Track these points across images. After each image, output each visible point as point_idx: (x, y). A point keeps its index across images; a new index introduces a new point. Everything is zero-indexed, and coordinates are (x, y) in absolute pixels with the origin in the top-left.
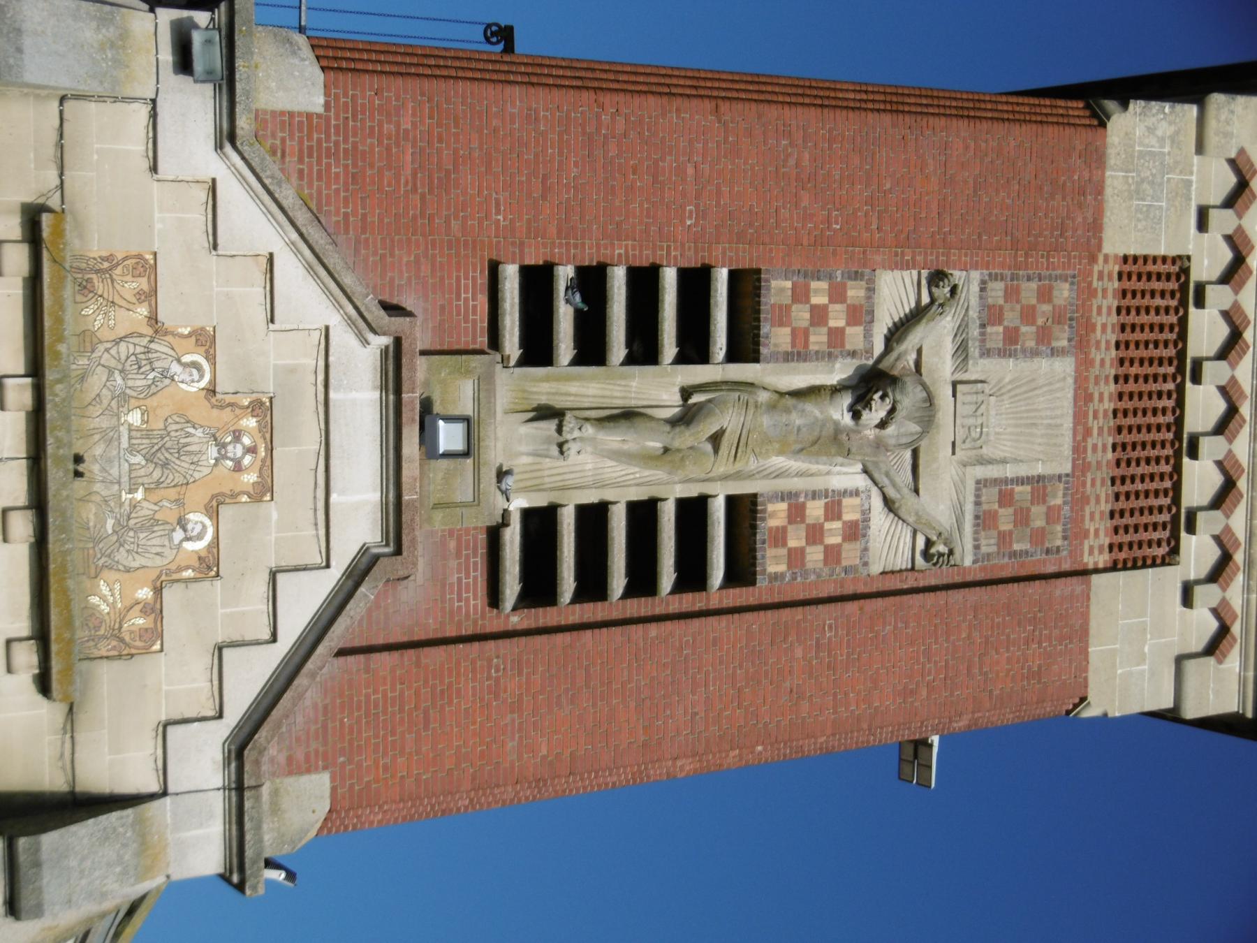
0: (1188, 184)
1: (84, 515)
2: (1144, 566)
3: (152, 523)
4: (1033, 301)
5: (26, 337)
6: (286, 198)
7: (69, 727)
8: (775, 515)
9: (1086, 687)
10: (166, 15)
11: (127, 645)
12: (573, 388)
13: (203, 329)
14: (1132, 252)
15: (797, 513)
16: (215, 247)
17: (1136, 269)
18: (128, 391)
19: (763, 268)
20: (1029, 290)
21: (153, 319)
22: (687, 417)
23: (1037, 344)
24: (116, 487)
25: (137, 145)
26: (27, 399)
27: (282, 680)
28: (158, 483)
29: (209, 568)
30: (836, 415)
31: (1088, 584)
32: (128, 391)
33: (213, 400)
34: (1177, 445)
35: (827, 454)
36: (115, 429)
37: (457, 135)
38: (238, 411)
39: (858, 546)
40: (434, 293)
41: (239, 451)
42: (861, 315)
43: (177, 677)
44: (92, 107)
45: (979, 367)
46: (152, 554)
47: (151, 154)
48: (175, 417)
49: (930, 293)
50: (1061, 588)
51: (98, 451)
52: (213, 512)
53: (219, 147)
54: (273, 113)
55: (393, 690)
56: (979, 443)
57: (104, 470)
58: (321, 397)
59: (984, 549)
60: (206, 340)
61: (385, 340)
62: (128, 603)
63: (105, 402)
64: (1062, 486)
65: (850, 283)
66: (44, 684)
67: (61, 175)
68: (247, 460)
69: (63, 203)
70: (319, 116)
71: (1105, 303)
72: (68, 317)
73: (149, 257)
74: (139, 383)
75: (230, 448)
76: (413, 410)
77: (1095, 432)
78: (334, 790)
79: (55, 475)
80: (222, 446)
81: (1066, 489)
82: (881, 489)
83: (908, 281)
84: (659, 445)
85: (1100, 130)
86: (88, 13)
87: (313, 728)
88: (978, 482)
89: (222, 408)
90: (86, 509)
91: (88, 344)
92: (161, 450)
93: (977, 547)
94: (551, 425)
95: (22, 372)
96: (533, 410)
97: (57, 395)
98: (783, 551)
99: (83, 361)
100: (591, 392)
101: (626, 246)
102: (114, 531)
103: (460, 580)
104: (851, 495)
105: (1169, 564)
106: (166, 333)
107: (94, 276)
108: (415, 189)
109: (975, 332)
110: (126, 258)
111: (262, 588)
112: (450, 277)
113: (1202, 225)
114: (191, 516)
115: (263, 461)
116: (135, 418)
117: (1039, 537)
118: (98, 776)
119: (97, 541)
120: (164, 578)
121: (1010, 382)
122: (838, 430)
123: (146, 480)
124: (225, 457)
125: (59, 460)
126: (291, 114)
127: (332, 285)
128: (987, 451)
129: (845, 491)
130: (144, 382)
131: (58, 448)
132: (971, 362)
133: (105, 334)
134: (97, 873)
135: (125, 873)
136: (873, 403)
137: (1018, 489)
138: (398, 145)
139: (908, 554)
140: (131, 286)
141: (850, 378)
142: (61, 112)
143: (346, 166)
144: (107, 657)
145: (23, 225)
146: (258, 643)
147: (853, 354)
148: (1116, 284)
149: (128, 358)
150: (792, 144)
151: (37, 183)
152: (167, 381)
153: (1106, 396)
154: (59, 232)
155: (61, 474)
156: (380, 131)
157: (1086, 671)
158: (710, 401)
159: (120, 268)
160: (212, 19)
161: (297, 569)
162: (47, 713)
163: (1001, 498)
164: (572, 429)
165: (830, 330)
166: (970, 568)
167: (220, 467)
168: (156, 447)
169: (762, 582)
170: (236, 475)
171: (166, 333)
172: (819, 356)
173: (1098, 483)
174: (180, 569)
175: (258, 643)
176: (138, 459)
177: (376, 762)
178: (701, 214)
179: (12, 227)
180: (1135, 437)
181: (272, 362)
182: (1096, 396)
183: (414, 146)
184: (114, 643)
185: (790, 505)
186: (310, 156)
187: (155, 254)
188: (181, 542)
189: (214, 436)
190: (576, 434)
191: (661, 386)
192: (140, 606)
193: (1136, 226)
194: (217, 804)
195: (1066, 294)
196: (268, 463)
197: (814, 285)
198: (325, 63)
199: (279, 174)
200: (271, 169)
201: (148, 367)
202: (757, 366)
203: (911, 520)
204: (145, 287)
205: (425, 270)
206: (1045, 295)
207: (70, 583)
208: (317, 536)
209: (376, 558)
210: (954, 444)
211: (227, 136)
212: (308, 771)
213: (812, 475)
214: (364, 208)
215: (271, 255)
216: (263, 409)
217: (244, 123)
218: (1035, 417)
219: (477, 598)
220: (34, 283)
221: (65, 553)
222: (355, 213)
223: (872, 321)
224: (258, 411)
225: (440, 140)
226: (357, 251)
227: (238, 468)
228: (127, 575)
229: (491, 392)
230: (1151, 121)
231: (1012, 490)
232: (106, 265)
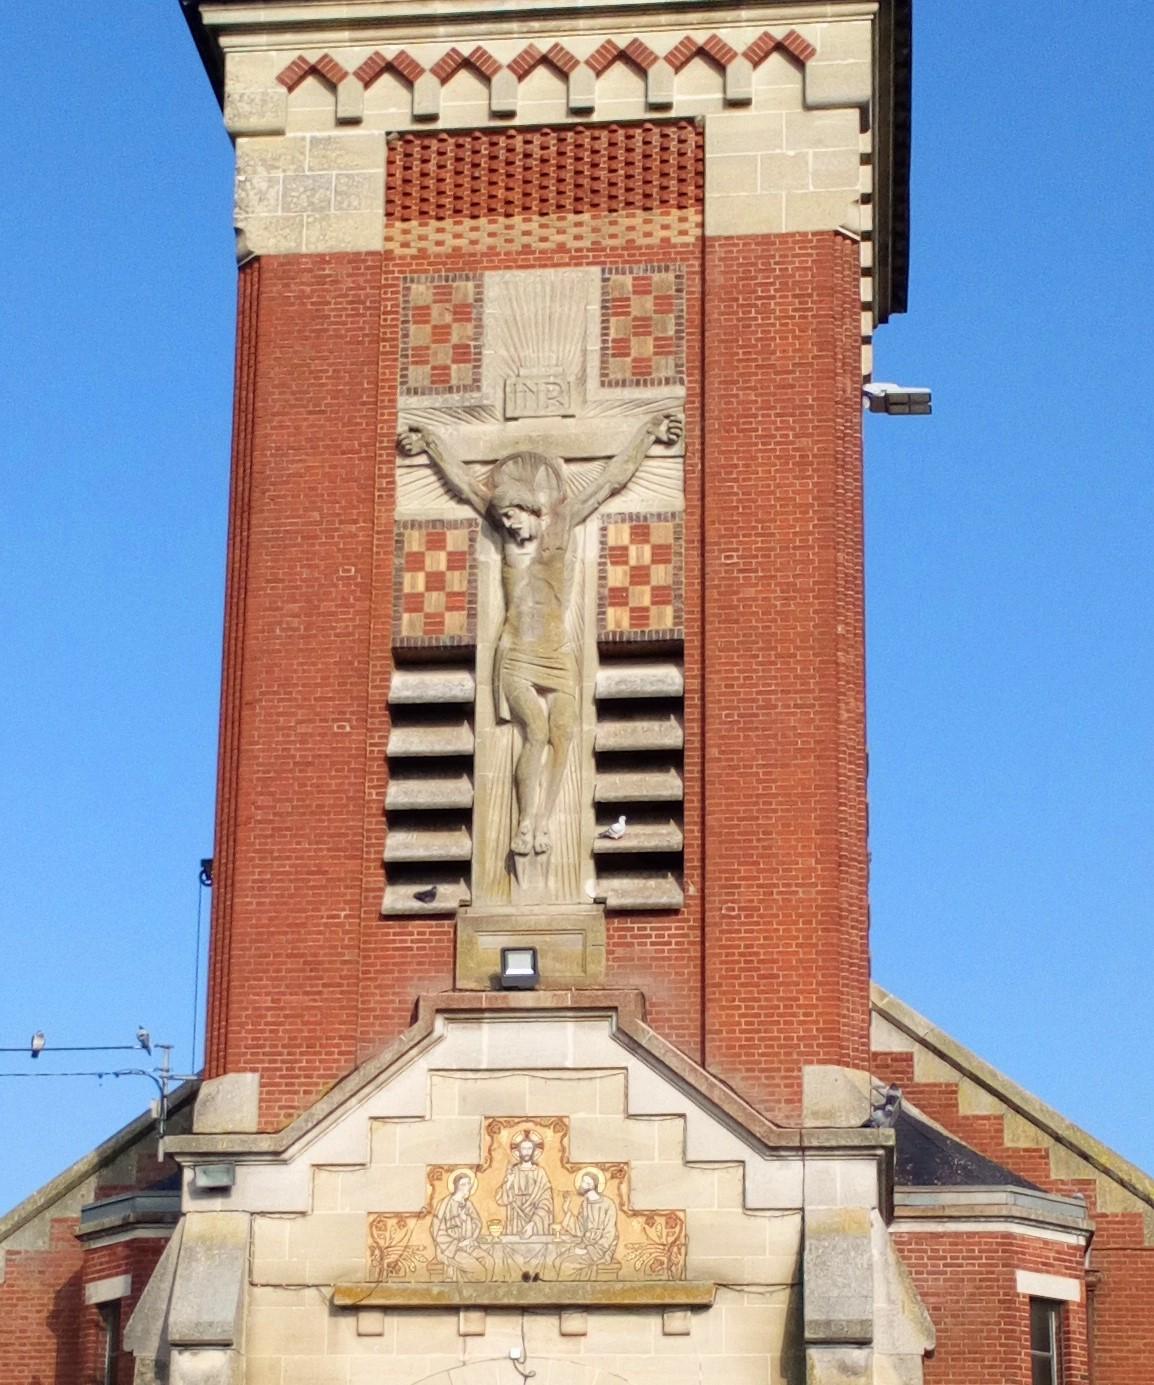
0: (315, 141)
2: (702, 160)
4: (428, 328)
6: (323, 1110)
7: (739, 1288)
8: (619, 621)
9: (821, 233)
14: (381, 211)
15: (618, 597)
19: (390, 646)
20: (419, 335)
21: (419, 1215)
23: (469, 320)
24: (550, 1246)
25: (287, 1228)
28: (549, 1212)
31: (714, 239)
33: (485, 1166)
34: (581, 128)
35: (561, 573)
36: (505, 1246)
37: (275, 956)
38: (495, 1146)
39: (654, 524)
40: (406, 971)
42: (435, 532)
43: (707, 1201)
44: (258, 1262)
45: (490, 392)
46: (604, 1213)
47: (292, 1216)
49: (418, 454)
51: (520, 1260)
52: (574, 1168)
53: (285, 1162)
54: (260, 1116)
55: (739, 1007)
56: (565, 387)
57: (536, 1256)
59: (671, 373)
60: (435, 1173)
64: (614, 277)
65: (406, 549)
67: (308, 1286)
70: (262, 1077)
74: (469, 1227)
75: (524, 1152)
76: (496, 998)
80: (522, 1159)
81: (617, 273)
82: (600, 504)
84: (546, 748)
85: (263, 261)
86: (186, 1269)
87: (764, 1081)
88: (603, 384)
90: (564, 1266)
92: (524, 1208)
93: (667, 381)
94: (519, 861)
96: (509, 874)
99: (450, 1270)
100: (496, 819)
101: (369, 787)
103: (652, 944)
104: (604, 536)
105: (704, 128)
106: (430, 1204)
107: (386, 1261)
108: (320, 993)
109: (455, 399)
112: (394, 957)
113: (354, 122)
114: (578, 1185)
115: (536, 1124)
117: (664, 304)
118: (780, 1268)
121: (508, 350)
122: (539, 560)
126: (261, 1100)
127: (393, 1068)
128: (574, 370)
129: (602, 543)
130: (469, 1222)
132: (485, 402)
133: (429, 1254)
134: (850, 1272)
135: (856, 1248)
136: (515, 526)
137: (613, 334)
138: (282, 1009)
139: (669, 463)
140: (394, 1235)
141: (494, 542)
142: (263, 1286)
143: (302, 1054)
147: (472, 540)
148: (414, 223)
149: (449, 1236)
150: (280, 623)
151: (313, 1305)
152: (469, 1204)
154: (347, 1292)
155: (532, 1293)
156: (273, 1024)
157: (805, 234)
158: (508, 700)
160: (189, 1167)
162: (725, 1305)
163: (622, 361)
164: (524, 842)
165: (449, 568)
166: (688, 389)
170: (547, 1147)
171: (430, 1204)
173: (613, 230)
176: (529, 1228)
177: (801, 1023)
178: (341, 715)
179: (347, 1323)
180: (569, 189)
183: (284, 994)
184: (675, 1249)
185: (613, 604)
186: (293, 1084)
187: (370, 1213)
188: (598, 1193)
190: (529, 838)
191: (491, 744)
193: (355, 209)
194: (816, 1166)
195: (422, 288)
197: (407, 589)
198: (221, 1070)
199: (304, 1115)
200: (299, 1123)
202: (479, 647)
203: (631, 467)
204: (395, 1221)
205: (388, 979)
206: (422, 314)
209: (619, 1029)
210: (564, 417)
211: (276, 1156)
212: (800, 1085)
213: (584, 581)
214: (334, 1038)
216: (493, 1126)
217: (265, 1143)
218: (543, 315)
219: (671, 925)
222: (338, 1046)
223: (442, 521)
225: (278, 971)
226: (371, 1041)
228: (621, 1239)
230: (253, 198)
231: (614, 341)
232: (377, 1252)
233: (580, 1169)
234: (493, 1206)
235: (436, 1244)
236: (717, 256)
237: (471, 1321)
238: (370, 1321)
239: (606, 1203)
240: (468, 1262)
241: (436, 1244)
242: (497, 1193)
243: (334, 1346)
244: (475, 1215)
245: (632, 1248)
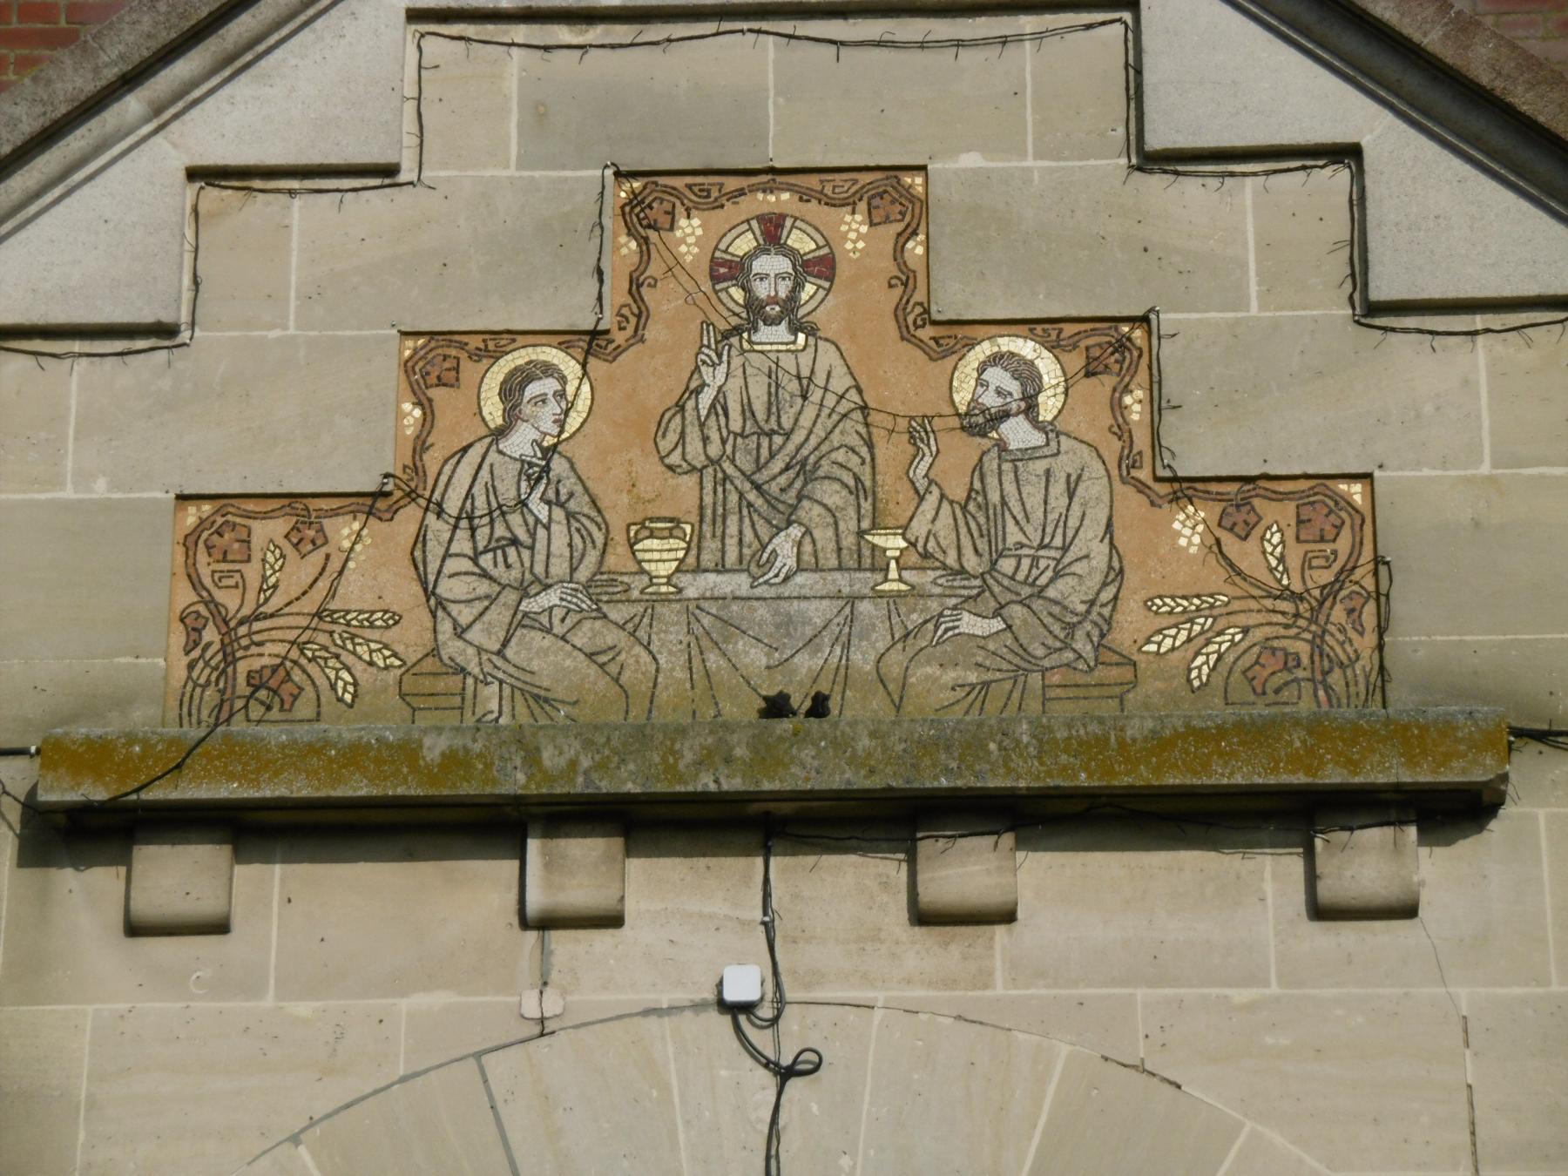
1: (948, 696)
5: (410, 856)
6: (13, 123)
11: (1347, 571)
13: (408, 367)
16: (164, 331)
18: (583, 574)
21: (372, 504)
24: (864, 607)
27: (1477, 123)
28: (858, 489)
29: (1122, 345)
32: (583, 574)
33: (620, 338)
38: (655, 268)
41: (773, 264)
46: (1063, 490)
48: (666, 445)
51: (754, 657)
52: (949, 336)
58: (622, 33)
60: (437, 360)
62: (1216, 576)
63: (612, 637)
66: (1455, 811)
68: (801, 242)
69: (21, 752)
72: (344, 730)
73: (192, 516)
75: (762, 290)
79: (810, 768)
80: (756, 312)
89: (642, 315)
90: (914, 668)
91: (441, 685)
92: (760, 480)
95: (514, 865)
97: (573, 764)
102: (996, 614)
106: (417, 469)
107: (243, 667)
110: (195, 582)
111: (1191, 195)
114: (962, 398)
115: (804, 196)
116: (661, 556)
119: (1023, 663)
120: (1144, 474)
123: (848, 525)
124: (790, 304)
125: (765, 755)
130: (559, 530)
131: (728, 760)
133: (411, 637)
140: (278, 571)
144: (1381, 631)
145: (81, 861)
146: (1358, 202)
149: (485, 575)
152: (558, 466)
155: (807, 754)
159: (219, 596)
161: (1136, 95)
167: (819, 317)
168: (752, 496)
170: (843, 271)
174: (1122, 431)
175: (1358, 202)
176: (785, 547)
179: (88, 893)
181: (512, 171)
184: (1338, 614)
187: (182, 498)
188: (1036, 424)
189: (726, 336)
192: (1228, 539)
196: (813, 181)
201: (515, 519)
204: (278, 527)
207: (1137, 728)
208: (1039, 36)
215: (193, 174)
220: (254, 829)
221: (1044, 741)
224: (657, 213)
227: (823, 267)
232: (210, 634)
233: (971, 345)
234: (649, 472)
235: (436, 604)
236: (469, 744)
237: (569, 869)
238: (175, 874)
239: (1071, 458)
240: (544, 670)
241: (436, 604)
242: (661, 427)
243: (31, 973)
244: (580, 504)
245: (1181, 624)
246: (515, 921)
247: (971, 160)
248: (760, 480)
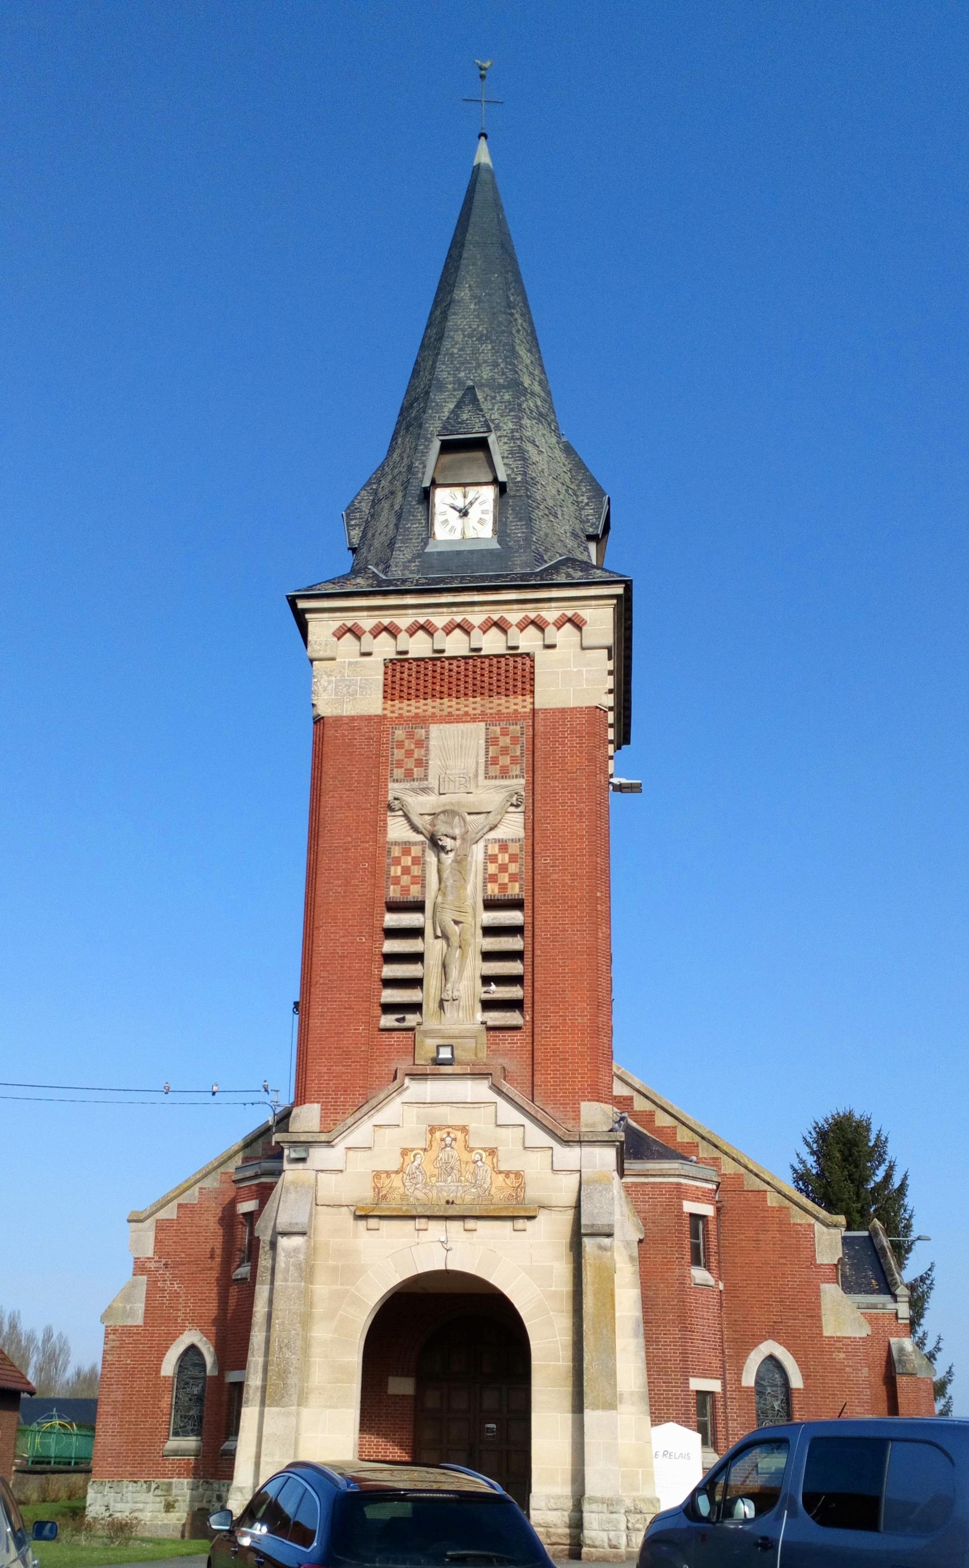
2: (533, 673)
3: (474, 1174)
8: (493, 890)
9: (590, 707)
10: (286, 1166)
12: (432, 991)
14: (381, 696)
15: (493, 878)
17: (391, 691)
20: (399, 754)
21: (397, 1172)
22: (445, 936)
25: (333, 1177)
26: (424, 1221)
30: (449, 861)
39: (510, 844)
42: (406, 847)
43: (534, 1167)
44: (319, 1194)
45: (433, 781)
46: (485, 1170)
50: (540, 728)
51: (445, 1194)
52: (471, 1150)
53: (333, 1146)
59: (518, 773)
60: (405, 1152)
61: (407, 1080)
62: (504, 1184)
68: (452, 1136)
71: (406, 708)
77: (466, 709)
78: (589, 1100)
83: (393, 822)
90: (466, 1197)
92: (447, 1169)
94: (445, 1004)
98: (510, 884)
109: (416, 784)
113: (369, 654)
118: (571, 1200)
125: (445, 1210)
126: (322, 1117)
133: (401, 1191)
135: (606, 1190)
137: (491, 754)
139: (517, 815)
140: (385, 1181)
147: (424, 851)
153: (449, 704)
154: (362, 1209)
162: (543, 1216)
163: (495, 766)
169: (523, 895)
172: (423, 870)
173: (491, 705)
176: (449, 1179)
179: (362, 1224)
182: (449, 710)
194: (587, 1150)
195: (400, 732)
197: (392, 874)
200: (340, 1127)
203: (499, 817)
205: (382, 1059)
206: (400, 745)
211: (329, 1144)
216: (432, 1130)
217: (323, 1137)
219: (518, 1035)
220: (381, 1217)
229: (431, 1031)
235: (405, 1186)
238: (373, 1223)
239: (486, 1167)
240: (419, 1195)
241: (405, 1186)
246: (579, 646)
247: (474, 1125)
248: (447, 1169)
